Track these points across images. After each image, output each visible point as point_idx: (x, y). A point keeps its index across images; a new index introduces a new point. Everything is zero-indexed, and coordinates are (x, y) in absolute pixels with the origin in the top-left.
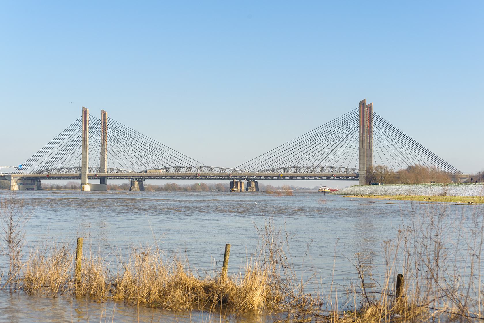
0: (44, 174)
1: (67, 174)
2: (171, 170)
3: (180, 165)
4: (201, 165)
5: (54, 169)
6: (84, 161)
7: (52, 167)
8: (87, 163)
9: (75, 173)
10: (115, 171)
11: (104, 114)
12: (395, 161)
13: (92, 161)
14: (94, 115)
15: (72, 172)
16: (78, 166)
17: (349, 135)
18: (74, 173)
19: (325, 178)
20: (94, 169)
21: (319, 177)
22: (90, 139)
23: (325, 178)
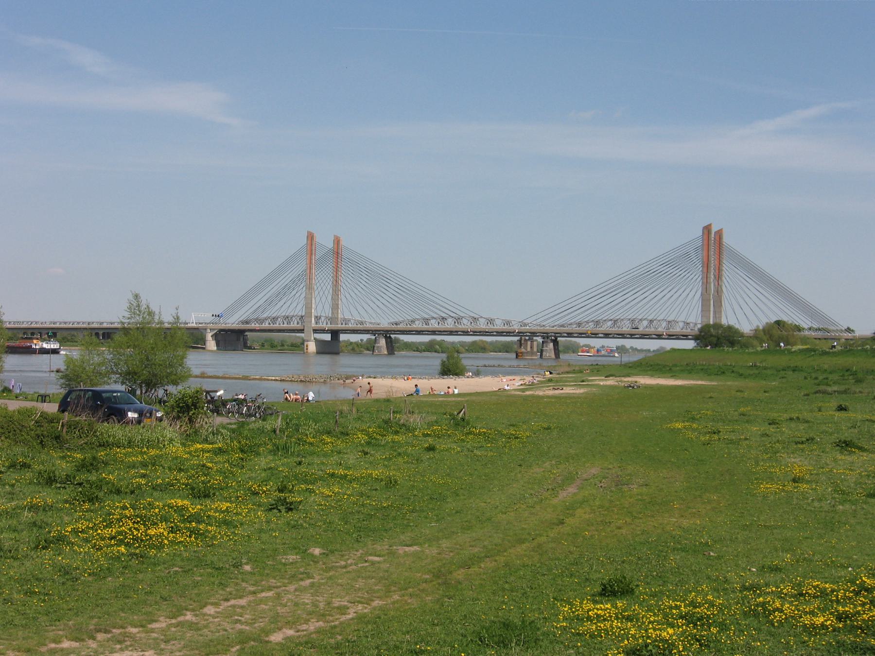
0: (253, 325)
1: (284, 325)
2: (433, 321)
3: (462, 315)
4: (476, 316)
5: (266, 319)
6: (308, 307)
7: (265, 316)
8: (313, 311)
9: (296, 325)
10: (482, 321)
11: (337, 241)
12: (679, 315)
13: (320, 307)
14: (325, 241)
15: (292, 323)
16: (300, 314)
17: (686, 277)
18: (294, 325)
19: (602, 335)
20: (323, 318)
21: (683, 336)
22: (318, 276)
23: (628, 336)
